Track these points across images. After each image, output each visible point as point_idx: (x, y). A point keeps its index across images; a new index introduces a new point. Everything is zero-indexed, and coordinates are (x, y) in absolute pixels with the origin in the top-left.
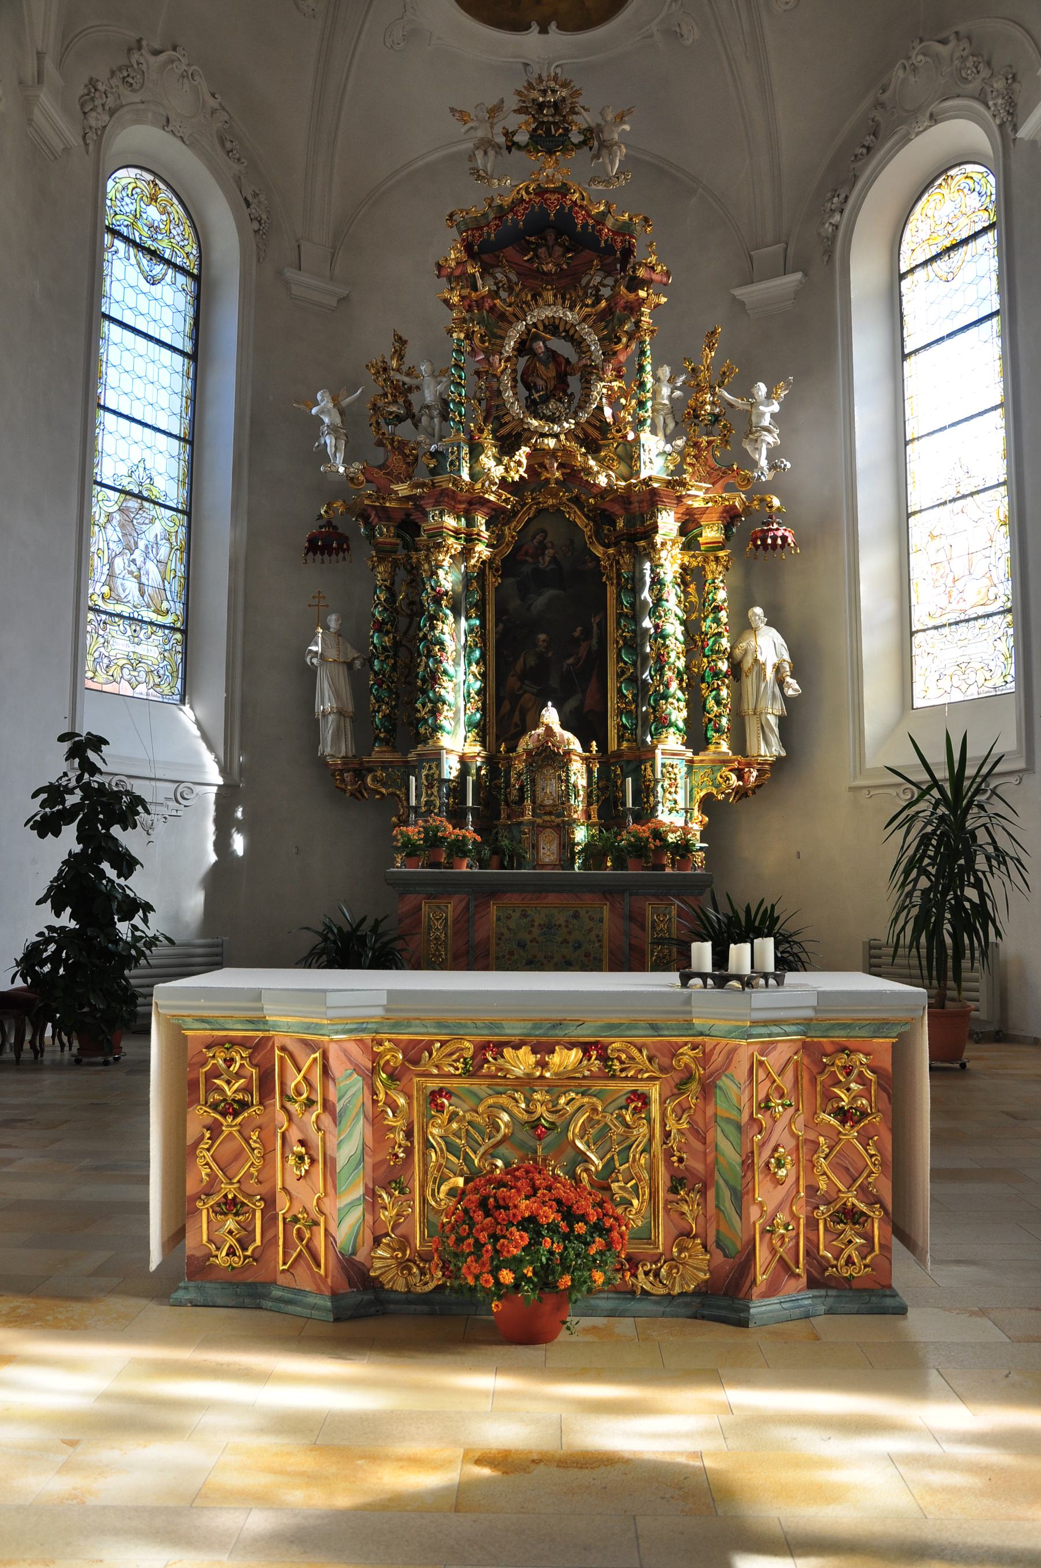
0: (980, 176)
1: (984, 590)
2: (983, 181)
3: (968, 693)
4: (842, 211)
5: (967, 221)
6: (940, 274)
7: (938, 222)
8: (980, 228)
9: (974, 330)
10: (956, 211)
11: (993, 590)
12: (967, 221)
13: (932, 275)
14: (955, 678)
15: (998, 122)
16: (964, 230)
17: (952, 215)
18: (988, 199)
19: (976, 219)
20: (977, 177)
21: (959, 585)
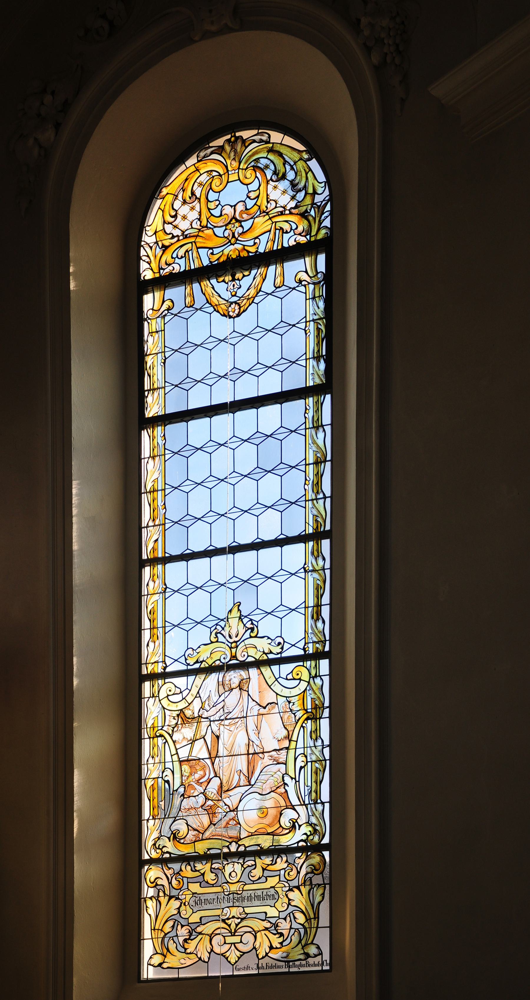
0: (296, 156)
1: (273, 813)
2: (300, 164)
3: (240, 964)
4: (57, 126)
5: (268, 225)
6: (215, 300)
7: (216, 212)
8: (182, 770)
9: (283, 339)
10: (250, 204)
11: (289, 814)
12: (268, 225)
13: (200, 300)
14: (215, 940)
15: (375, 59)
16: (264, 238)
17: (240, 207)
18: (308, 201)
19: (286, 227)
20: (291, 156)
21: (232, 799)
